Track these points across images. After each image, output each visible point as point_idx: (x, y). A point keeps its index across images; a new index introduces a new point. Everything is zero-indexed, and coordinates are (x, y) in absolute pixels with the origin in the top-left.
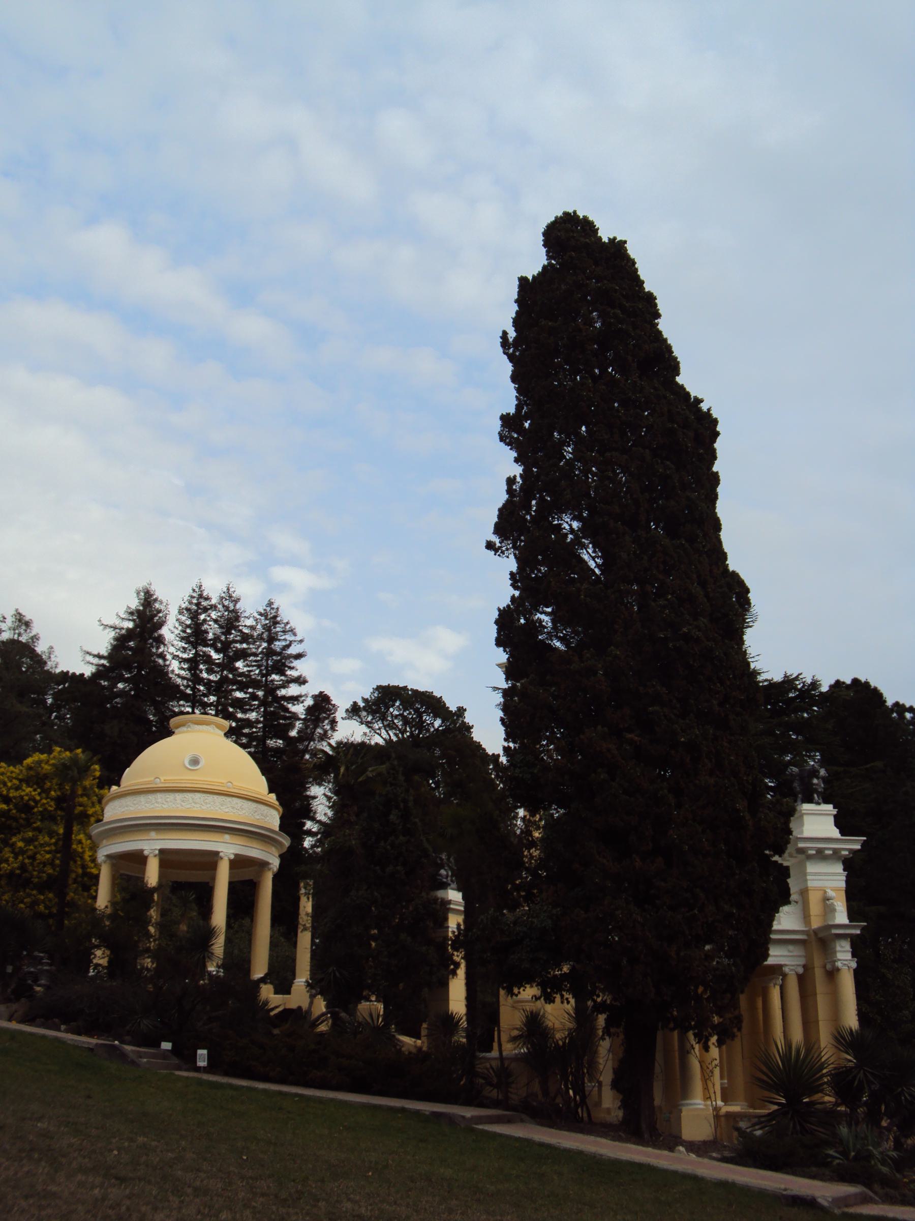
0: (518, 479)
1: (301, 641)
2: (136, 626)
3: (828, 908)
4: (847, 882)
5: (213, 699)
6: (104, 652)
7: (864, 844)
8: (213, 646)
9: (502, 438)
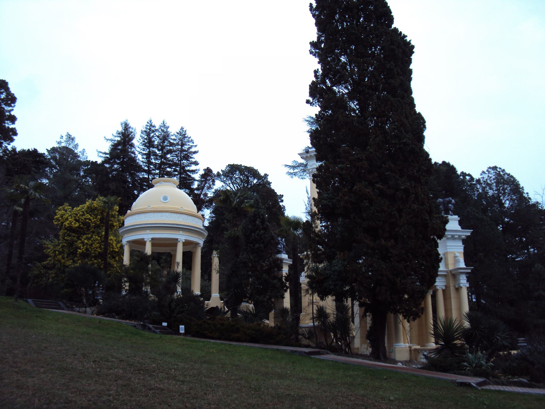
0: (320, 70)
1: (196, 146)
2: (122, 139)
3: (456, 261)
4: (464, 249)
5: (157, 171)
6: (108, 152)
7: (472, 233)
8: (157, 148)
9: (311, 53)
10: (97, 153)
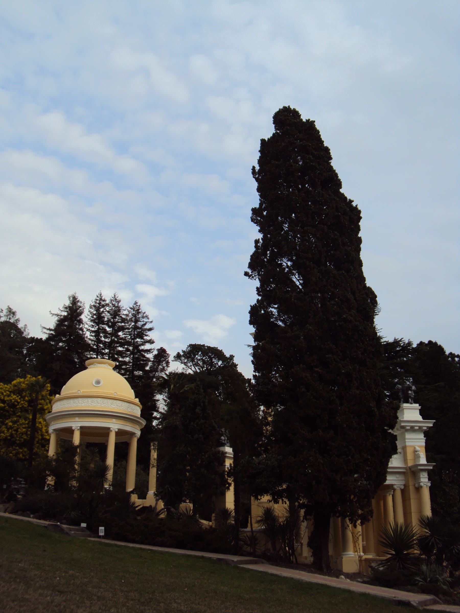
0: (261, 240)
1: (151, 322)
2: (68, 314)
3: (416, 456)
4: (426, 443)
5: (107, 351)
6: (52, 328)
7: (434, 424)
8: (107, 324)
10: (41, 328)
